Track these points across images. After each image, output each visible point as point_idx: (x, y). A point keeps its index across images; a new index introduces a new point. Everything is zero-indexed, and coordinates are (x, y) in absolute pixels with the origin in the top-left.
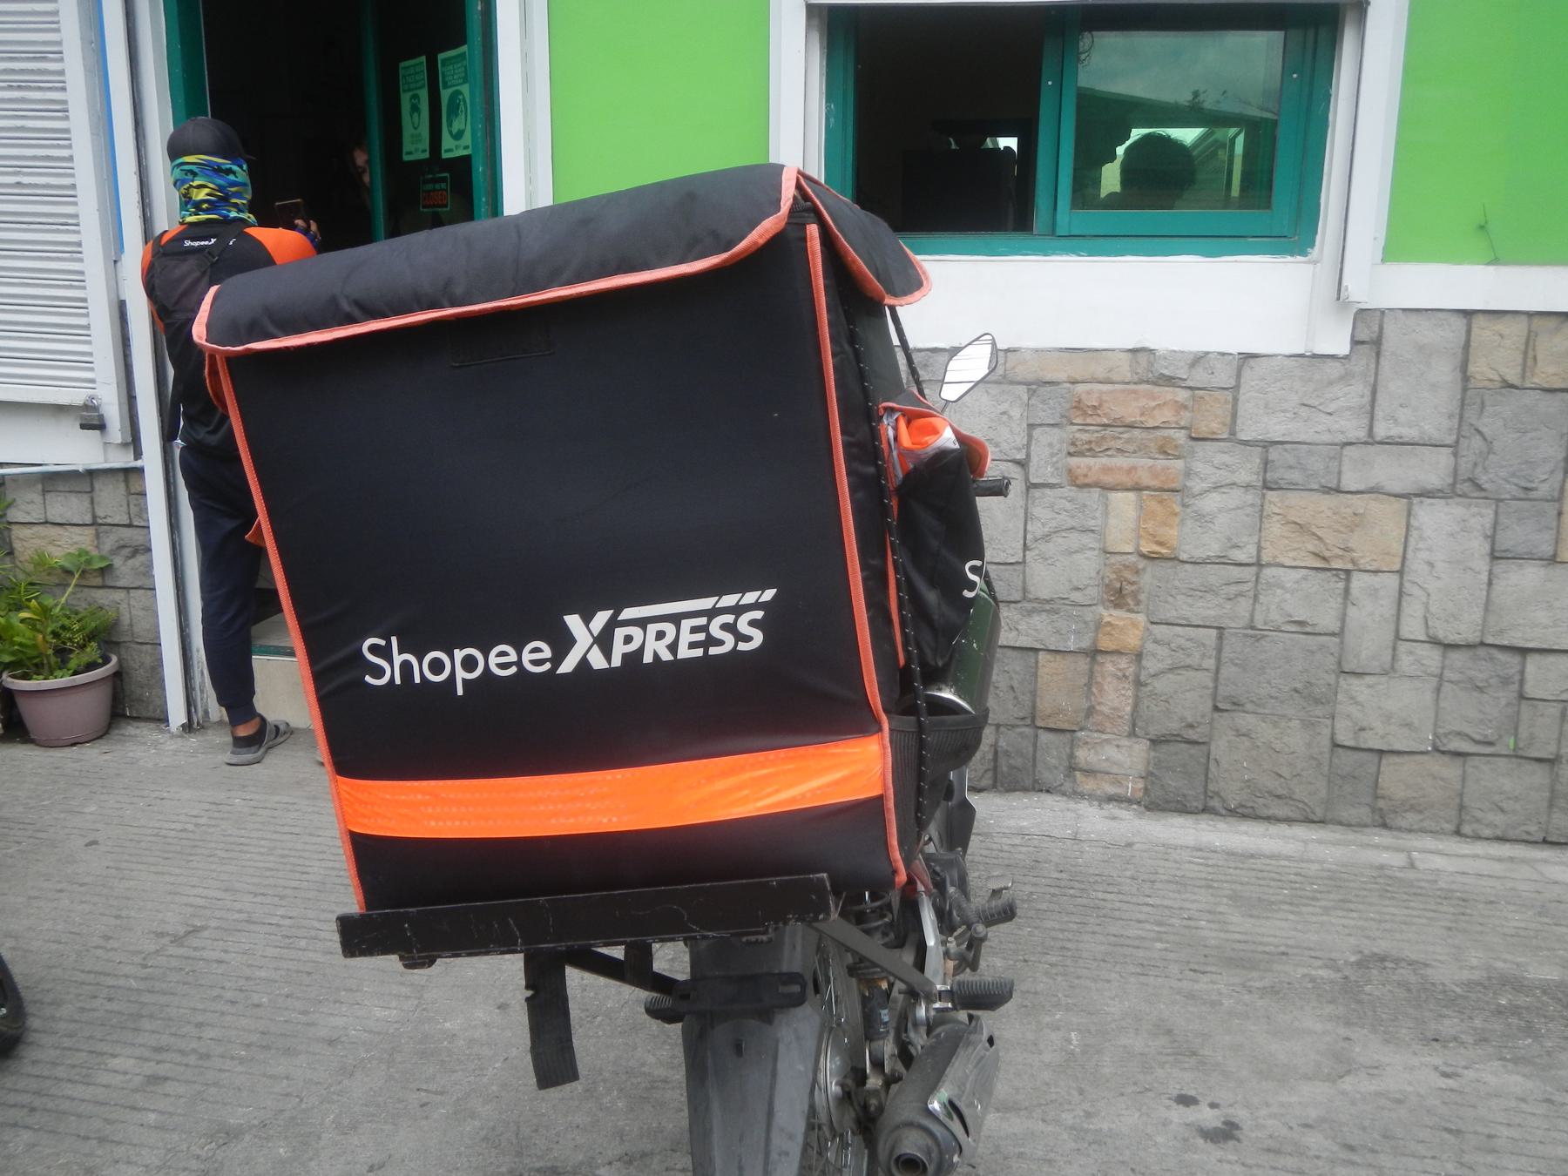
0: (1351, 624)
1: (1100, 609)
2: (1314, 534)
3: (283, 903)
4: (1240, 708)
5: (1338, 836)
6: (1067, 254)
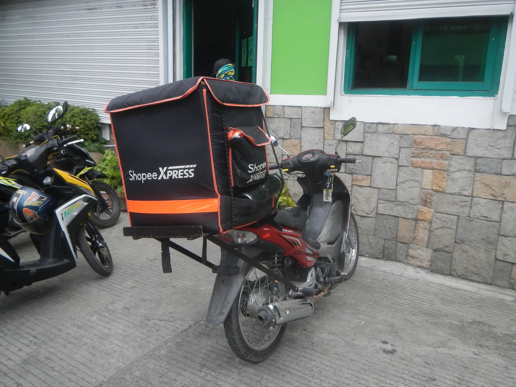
0: (503, 219)
1: (420, 206)
2: (491, 188)
3: (178, 257)
4: (464, 243)
5: (494, 289)
6: (415, 95)
